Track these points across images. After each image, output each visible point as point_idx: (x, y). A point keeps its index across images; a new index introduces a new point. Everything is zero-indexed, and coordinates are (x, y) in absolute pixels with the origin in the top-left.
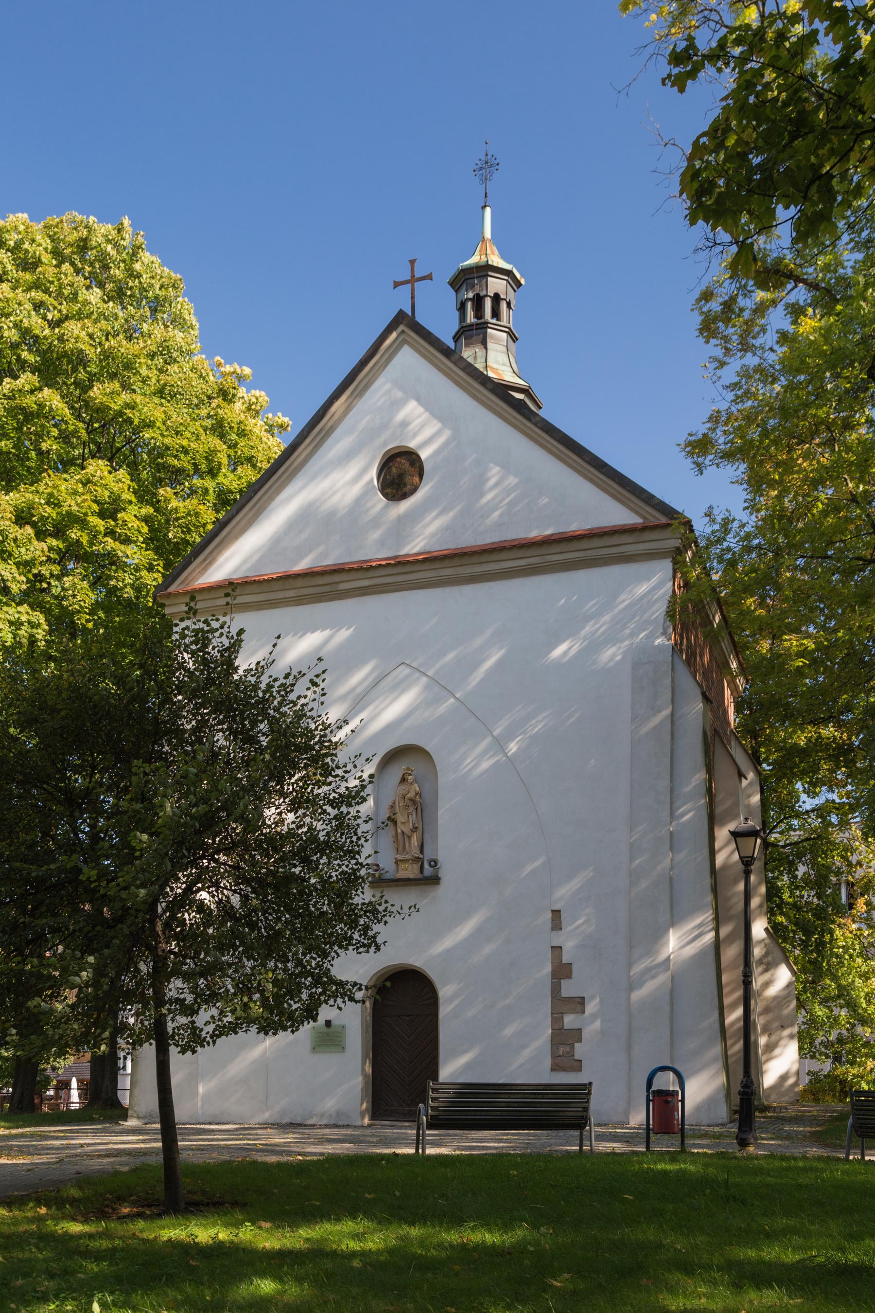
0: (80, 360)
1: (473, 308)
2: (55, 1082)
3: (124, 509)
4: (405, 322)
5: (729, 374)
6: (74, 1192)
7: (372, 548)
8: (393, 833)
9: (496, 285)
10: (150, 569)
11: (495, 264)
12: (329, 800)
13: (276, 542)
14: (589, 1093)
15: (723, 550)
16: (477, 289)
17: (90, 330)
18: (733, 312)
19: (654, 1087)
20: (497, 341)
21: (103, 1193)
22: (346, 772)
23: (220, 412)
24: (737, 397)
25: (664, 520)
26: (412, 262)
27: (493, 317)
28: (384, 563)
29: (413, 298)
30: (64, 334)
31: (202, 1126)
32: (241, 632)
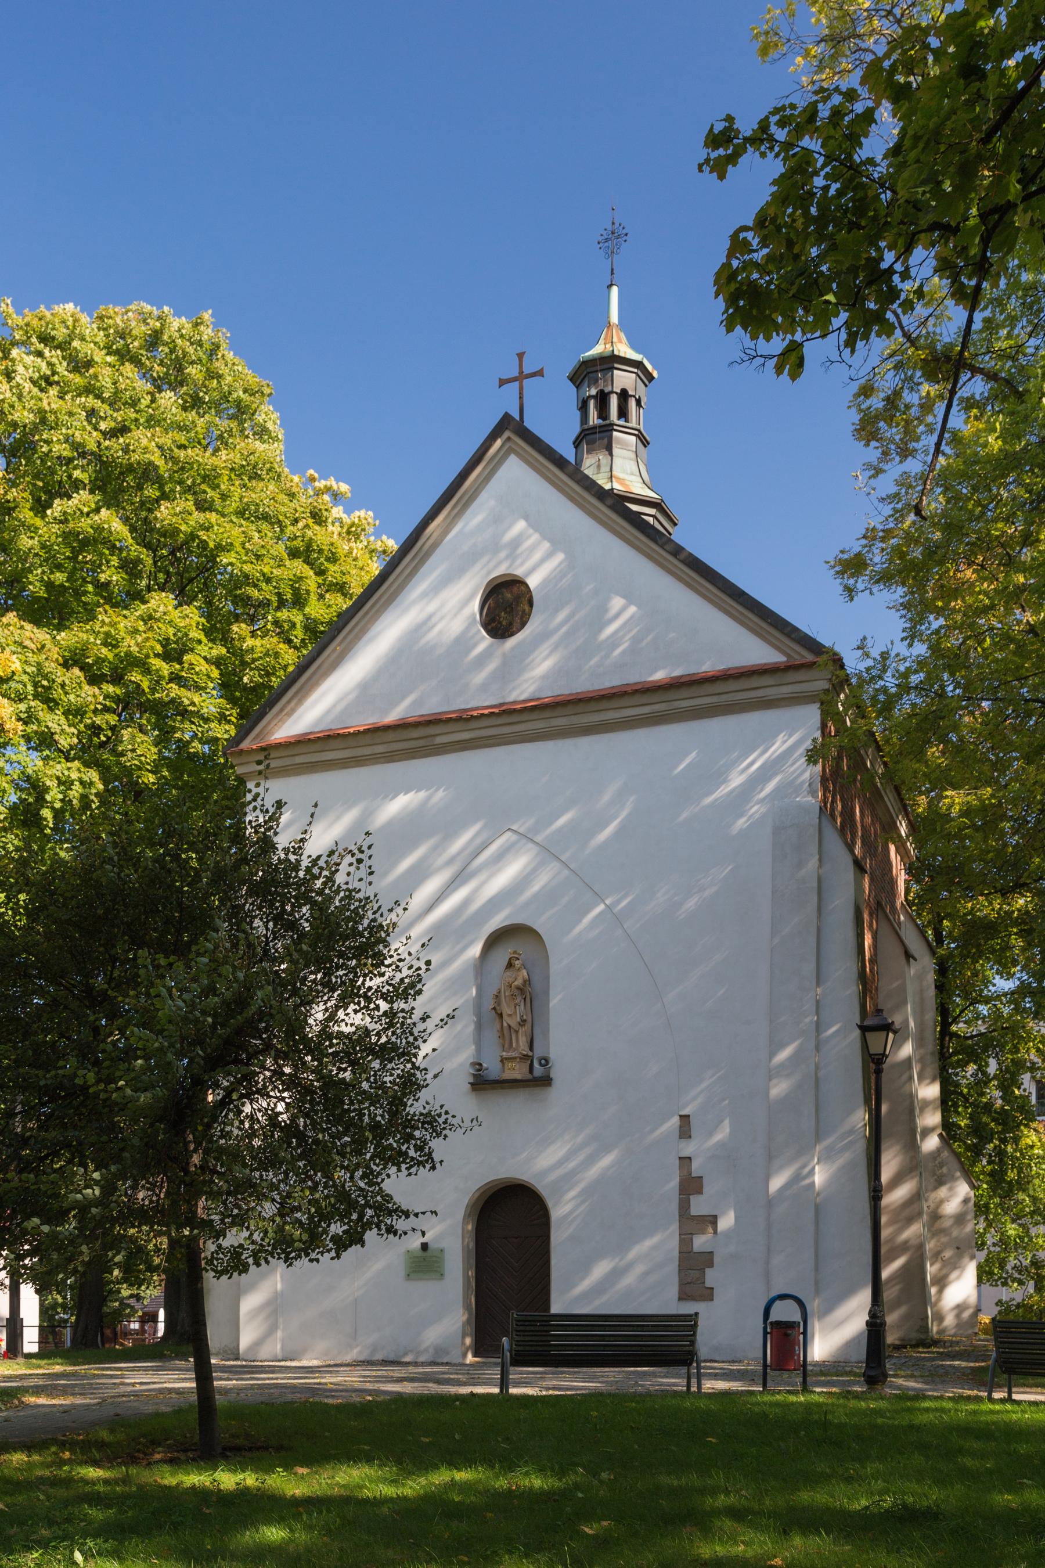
0: (147, 473)
1: (596, 407)
2: (140, 1313)
3: (192, 650)
4: (512, 428)
5: (886, 485)
6: (105, 1435)
7: (477, 692)
8: (498, 1026)
9: (623, 379)
10: (222, 718)
11: (622, 355)
12: (383, 994)
13: (364, 687)
14: (696, 1325)
15: (877, 690)
16: (601, 384)
17: (161, 441)
18: (896, 408)
19: (774, 1317)
20: (624, 446)
21: (134, 1436)
22: (400, 960)
23: (309, 533)
24: (896, 511)
25: (810, 657)
26: (521, 356)
27: (619, 418)
28: (486, 712)
29: (521, 398)
30: (128, 445)
31: (282, 1364)
32: (279, 805)
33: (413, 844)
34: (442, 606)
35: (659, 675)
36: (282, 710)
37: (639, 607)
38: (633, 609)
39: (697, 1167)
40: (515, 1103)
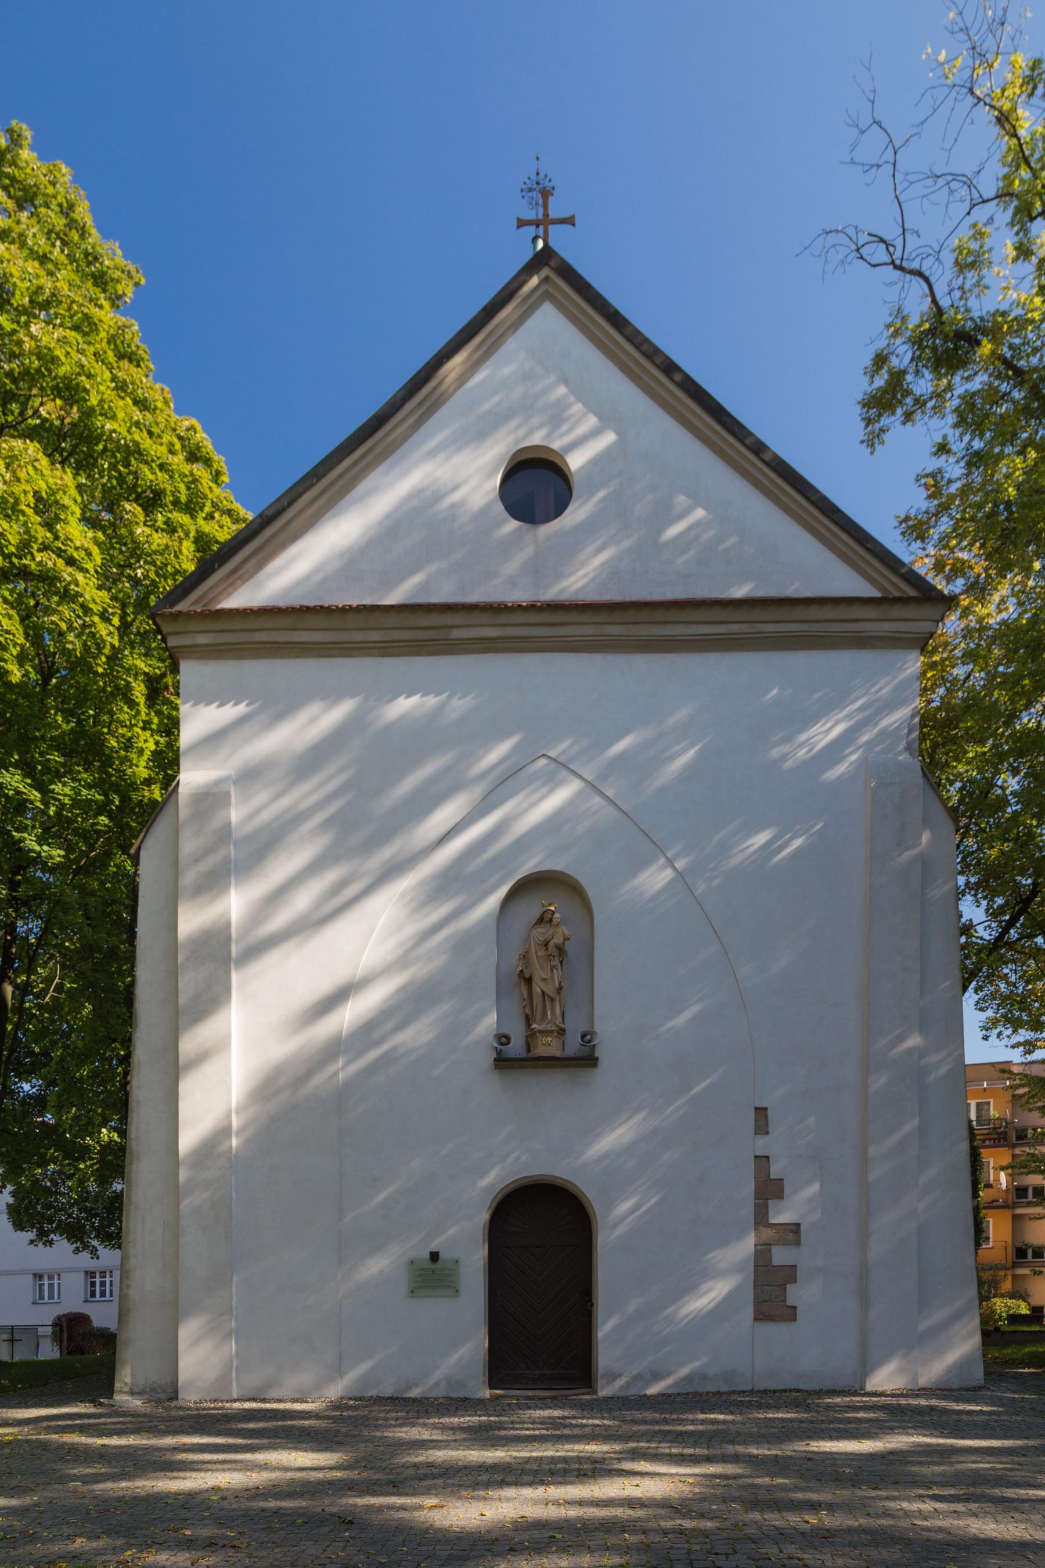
7: (508, 582)
25: (912, 593)
33: (418, 758)
34: (453, 470)
35: (740, 592)
36: (234, 571)
37: (706, 509)
39: (776, 1170)
40: (554, 1082)
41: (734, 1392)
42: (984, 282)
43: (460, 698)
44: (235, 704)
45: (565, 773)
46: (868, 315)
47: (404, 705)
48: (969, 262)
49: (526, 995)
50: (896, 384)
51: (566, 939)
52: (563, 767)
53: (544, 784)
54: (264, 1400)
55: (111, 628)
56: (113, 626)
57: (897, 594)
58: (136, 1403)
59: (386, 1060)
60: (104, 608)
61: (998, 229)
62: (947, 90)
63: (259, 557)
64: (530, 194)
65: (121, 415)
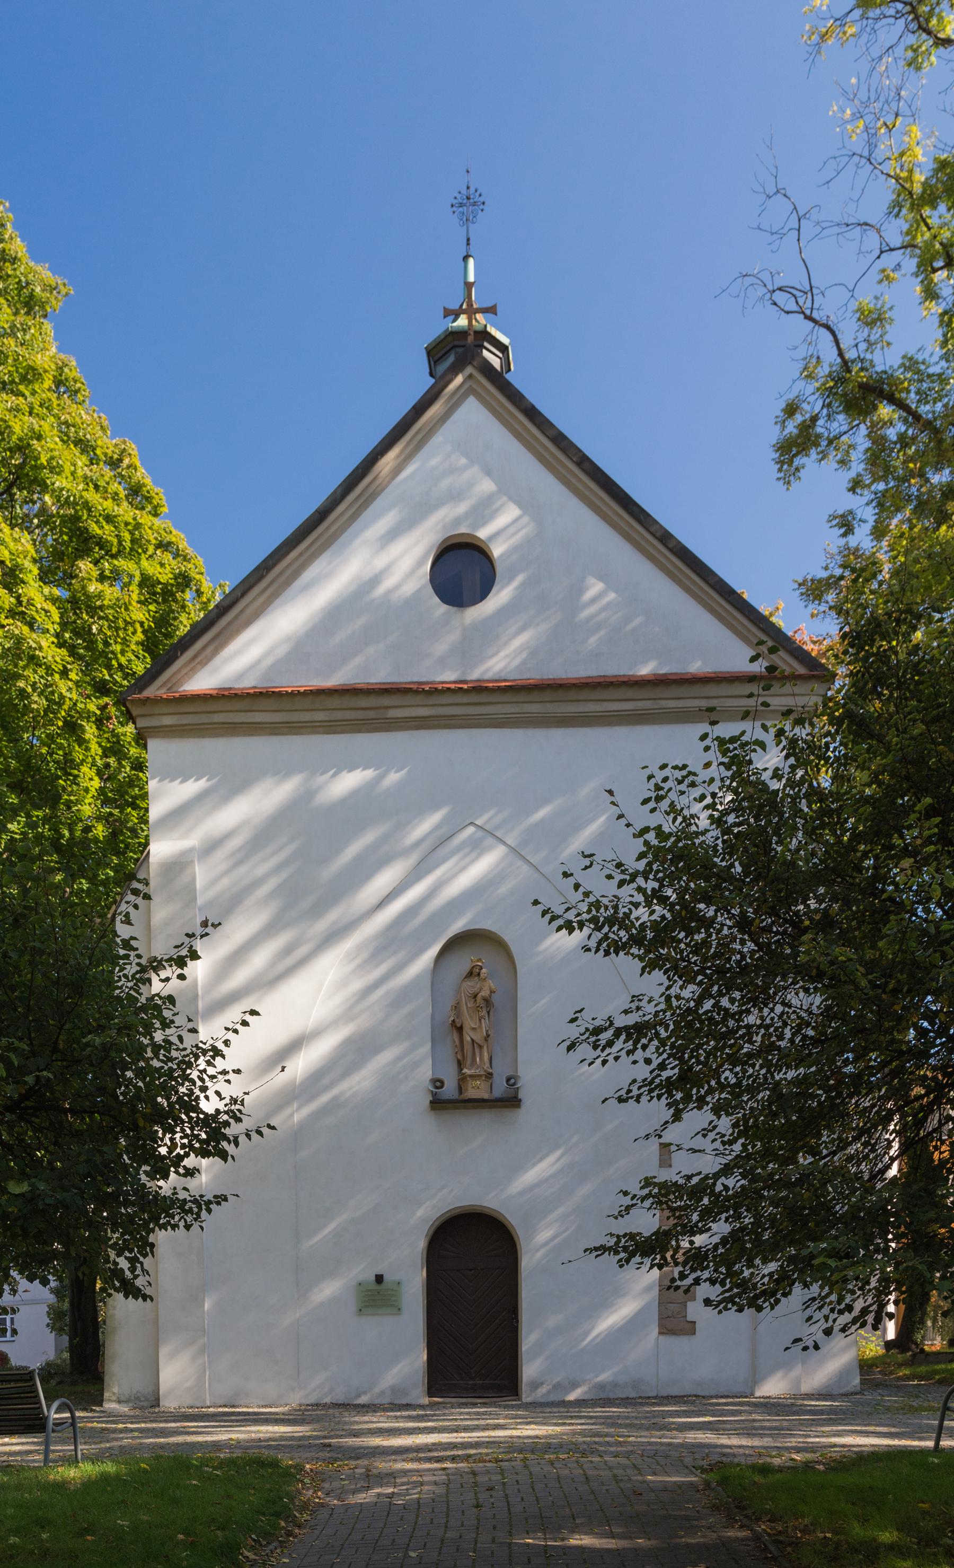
25: (801, 670)
28: (453, 686)
34: (386, 557)
35: (645, 670)
36: (195, 657)
37: (616, 592)
38: (612, 596)
40: (483, 1121)
41: (640, 1397)
42: (887, 338)
43: (396, 772)
44: (196, 780)
45: (490, 840)
46: (778, 366)
47: (348, 782)
48: (873, 319)
49: (457, 1041)
50: (807, 427)
51: (492, 992)
52: (490, 834)
53: (472, 851)
54: (233, 1406)
55: (70, 683)
56: (71, 680)
57: (788, 671)
58: (124, 1409)
59: (334, 1106)
60: (64, 666)
61: (905, 275)
62: (847, 159)
63: (216, 643)
64: (461, 209)
65: (68, 468)
